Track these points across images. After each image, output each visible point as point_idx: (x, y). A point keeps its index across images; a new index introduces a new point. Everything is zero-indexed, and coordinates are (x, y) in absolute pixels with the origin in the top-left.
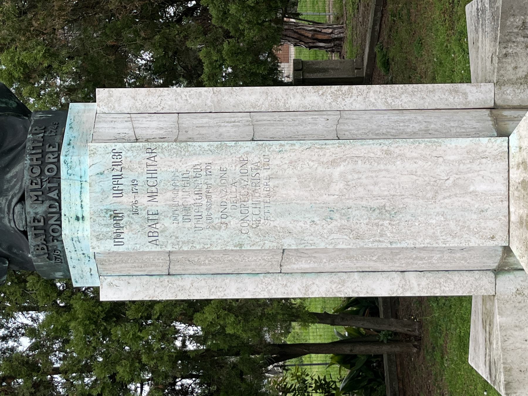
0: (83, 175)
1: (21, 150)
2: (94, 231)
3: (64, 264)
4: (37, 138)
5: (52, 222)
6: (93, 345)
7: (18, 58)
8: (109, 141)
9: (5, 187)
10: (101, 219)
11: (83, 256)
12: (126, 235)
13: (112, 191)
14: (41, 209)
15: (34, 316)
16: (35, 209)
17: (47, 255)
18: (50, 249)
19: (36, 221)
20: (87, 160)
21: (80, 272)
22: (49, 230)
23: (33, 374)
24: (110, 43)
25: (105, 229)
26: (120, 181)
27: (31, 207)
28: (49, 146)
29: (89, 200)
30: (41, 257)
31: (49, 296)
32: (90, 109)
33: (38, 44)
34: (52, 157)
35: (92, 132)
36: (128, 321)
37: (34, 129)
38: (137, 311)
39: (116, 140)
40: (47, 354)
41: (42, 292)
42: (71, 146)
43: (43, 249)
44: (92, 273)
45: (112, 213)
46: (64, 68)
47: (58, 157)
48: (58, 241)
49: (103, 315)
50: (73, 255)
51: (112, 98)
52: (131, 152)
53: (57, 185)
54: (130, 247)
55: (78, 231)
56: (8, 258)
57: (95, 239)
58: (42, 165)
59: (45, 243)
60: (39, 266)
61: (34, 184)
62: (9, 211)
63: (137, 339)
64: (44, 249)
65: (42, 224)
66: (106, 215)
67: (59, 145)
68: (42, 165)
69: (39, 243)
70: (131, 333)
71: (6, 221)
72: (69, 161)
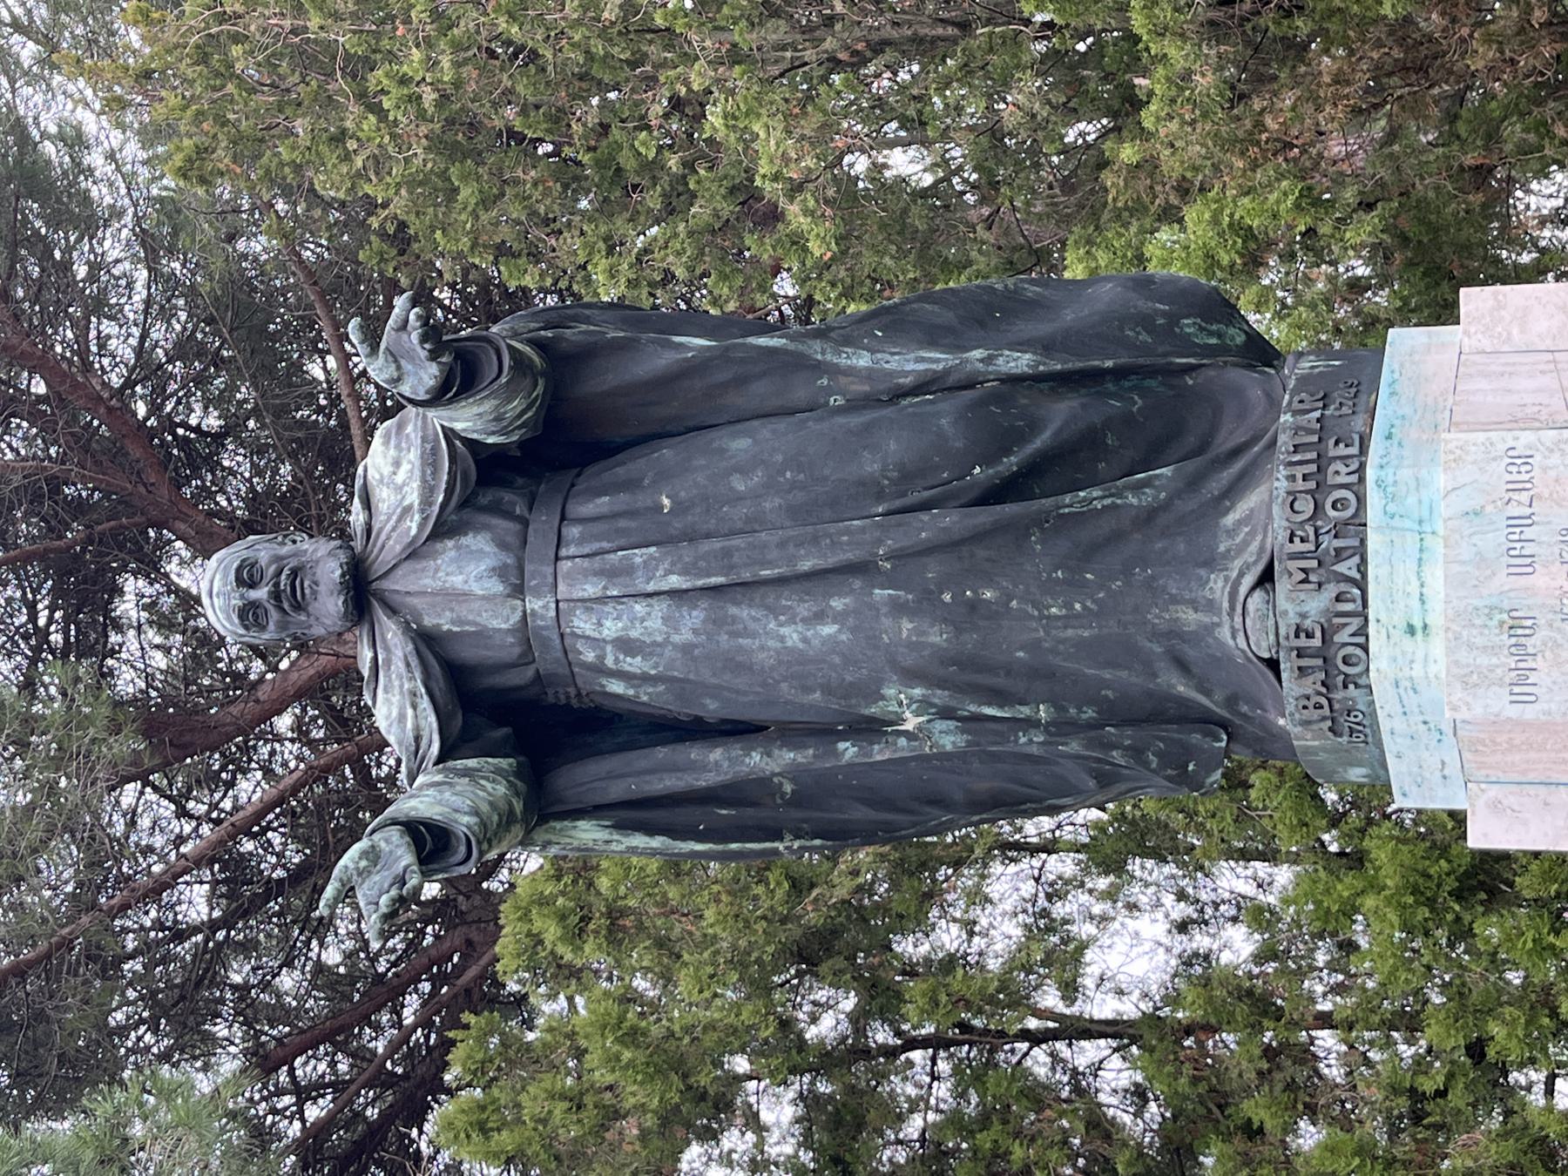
0: (1425, 514)
1: (1260, 453)
2: (1456, 663)
3: (1372, 747)
4: (1304, 423)
5: (1343, 637)
6: (1425, 960)
7: (1231, 216)
8: (1497, 425)
9: (1222, 548)
10: (1475, 632)
11: (1423, 728)
12: (1544, 674)
13: (1506, 560)
14: (1316, 604)
15: (1261, 874)
16: (1300, 604)
17: (1329, 723)
18: (1336, 706)
19: (1303, 635)
20: (1441, 480)
21: (1415, 769)
22: (1334, 658)
23: (1266, 1023)
24: (1469, 160)
25: (1484, 660)
26: (1529, 533)
27: (1288, 599)
28: (1337, 443)
29: (1441, 581)
30: (1315, 727)
31: (1306, 825)
32: (1443, 344)
33: (1281, 176)
34: (1344, 470)
35: (1449, 403)
36: (1518, 901)
37: (1296, 399)
38: (1548, 876)
39: (1517, 422)
40: (1301, 974)
41: (1289, 814)
42: (1395, 441)
43: (1319, 706)
44: (1446, 772)
45: (1505, 616)
46: (1348, 235)
47: (1361, 469)
48: (1357, 686)
49: (1451, 883)
50: (1399, 724)
51: (1503, 313)
52: (1557, 455)
53: (1357, 543)
54: (1553, 707)
55: (1412, 662)
56: (1224, 725)
57: (1459, 686)
58: (1320, 488)
59: (1324, 690)
60: (1307, 751)
61: (1297, 540)
62: (1232, 608)
63: (1545, 954)
64: (1321, 707)
65: (1317, 642)
66: (1490, 623)
67: (1361, 438)
68: (1320, 488)
69: (1309, 691)
70: (1530, 935)
71: (1225, 633)
72: (1390, 479)
